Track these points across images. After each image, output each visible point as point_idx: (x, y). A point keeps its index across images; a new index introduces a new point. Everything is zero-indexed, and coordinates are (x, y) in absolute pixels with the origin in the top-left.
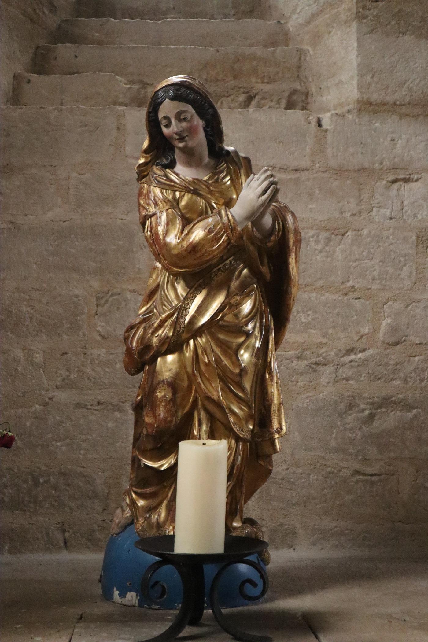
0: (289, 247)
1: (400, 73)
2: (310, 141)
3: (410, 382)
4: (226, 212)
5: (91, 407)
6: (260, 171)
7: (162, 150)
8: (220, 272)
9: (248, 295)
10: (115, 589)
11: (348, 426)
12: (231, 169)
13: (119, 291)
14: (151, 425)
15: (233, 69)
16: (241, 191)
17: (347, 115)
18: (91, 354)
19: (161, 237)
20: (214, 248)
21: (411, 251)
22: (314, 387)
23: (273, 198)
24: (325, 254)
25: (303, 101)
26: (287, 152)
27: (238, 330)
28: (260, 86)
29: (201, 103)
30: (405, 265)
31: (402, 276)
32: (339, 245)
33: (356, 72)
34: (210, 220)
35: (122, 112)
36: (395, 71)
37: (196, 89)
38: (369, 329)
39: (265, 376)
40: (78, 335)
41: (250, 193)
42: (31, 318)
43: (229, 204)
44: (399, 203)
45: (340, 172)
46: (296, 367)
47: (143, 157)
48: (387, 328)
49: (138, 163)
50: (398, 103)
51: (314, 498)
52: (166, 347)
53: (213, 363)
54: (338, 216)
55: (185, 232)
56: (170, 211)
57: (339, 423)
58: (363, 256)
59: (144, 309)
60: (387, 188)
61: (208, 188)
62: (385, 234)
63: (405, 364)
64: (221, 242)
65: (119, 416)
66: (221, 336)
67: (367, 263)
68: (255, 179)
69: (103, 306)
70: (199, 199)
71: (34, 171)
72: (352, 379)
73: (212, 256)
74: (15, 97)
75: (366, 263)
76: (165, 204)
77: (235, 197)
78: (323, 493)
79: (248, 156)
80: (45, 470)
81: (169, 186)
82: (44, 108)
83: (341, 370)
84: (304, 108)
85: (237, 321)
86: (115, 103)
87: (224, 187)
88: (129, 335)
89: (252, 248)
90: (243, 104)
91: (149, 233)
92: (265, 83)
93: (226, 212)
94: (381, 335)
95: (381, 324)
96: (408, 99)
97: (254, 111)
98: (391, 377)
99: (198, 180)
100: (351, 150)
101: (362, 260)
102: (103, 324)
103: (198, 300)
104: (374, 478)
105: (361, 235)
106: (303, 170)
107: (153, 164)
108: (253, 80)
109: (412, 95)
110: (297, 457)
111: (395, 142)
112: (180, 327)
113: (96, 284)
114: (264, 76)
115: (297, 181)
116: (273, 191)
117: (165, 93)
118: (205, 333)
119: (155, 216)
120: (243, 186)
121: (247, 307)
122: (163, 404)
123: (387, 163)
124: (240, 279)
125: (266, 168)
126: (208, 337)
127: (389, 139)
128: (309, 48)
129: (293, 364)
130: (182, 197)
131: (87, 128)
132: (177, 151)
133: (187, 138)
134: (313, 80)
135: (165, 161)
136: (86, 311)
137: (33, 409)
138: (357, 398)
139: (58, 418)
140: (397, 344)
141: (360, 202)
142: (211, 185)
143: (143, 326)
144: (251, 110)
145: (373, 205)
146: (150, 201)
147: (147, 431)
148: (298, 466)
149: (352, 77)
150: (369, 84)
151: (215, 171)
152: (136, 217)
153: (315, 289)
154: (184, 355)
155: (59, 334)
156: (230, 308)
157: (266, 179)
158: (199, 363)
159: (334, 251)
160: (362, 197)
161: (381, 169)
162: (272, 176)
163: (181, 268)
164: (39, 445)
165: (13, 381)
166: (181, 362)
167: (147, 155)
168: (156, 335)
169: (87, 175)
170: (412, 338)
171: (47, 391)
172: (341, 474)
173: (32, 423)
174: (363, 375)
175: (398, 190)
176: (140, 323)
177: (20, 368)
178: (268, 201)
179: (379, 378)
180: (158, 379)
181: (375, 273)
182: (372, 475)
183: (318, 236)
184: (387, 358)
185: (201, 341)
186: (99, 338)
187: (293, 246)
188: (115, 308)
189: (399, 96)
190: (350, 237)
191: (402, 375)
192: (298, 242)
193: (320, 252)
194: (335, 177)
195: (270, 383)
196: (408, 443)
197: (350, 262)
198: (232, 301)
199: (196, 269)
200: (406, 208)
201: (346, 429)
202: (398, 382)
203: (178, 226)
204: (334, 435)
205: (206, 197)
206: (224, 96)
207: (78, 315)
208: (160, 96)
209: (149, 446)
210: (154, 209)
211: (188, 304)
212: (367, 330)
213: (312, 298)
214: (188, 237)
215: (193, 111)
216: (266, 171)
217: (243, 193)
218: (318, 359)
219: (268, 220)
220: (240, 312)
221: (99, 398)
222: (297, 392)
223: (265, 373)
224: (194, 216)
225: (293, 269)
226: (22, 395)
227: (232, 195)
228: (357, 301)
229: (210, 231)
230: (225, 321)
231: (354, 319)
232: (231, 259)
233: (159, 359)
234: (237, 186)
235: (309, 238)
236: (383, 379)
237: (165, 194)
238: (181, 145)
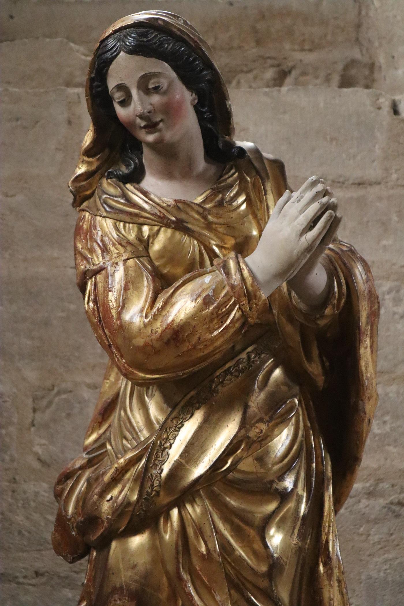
0: (359, 327)
2: (381, 137)
4: (238, 263)
6: (302, 183)
7: (118, 149)
8: (229, 377)
9: (283, 421)
12: (247, 181)
13: (69, 385)
15: (255, 30)
16: (266, 223)
18: (25, 492)
19: (114, 312)
20: (216, 333)
22: (395, 543)
23: (329, 234)
25: (366, 78)
26: (344, 156)
27: (265, 488)
28: (298, 56)
29: (188, 58)
34: (207, 279)
35: (76, 97)
37: (178, 33)
39: (318, 571)
41: (284, 226)
43: (243, 247)
46: (367, 510)
47: (83, 162)
49: (74, 172)
52: (126, 521)
53: (216, 555)
55: (159, 304)
56: (131, 262)
59: (94, 437)
61: (205, 218)
64: (228, 322)
65: (70, 595)
66: (233, 502)
68: (292, 200)
69: (43, 412)
70: (186, 239)
73: (211, 348)
76: (122, 250)
77: (255, 233)
79: (278, 157)
81: (133, 216)
84: (367, 87)
85: (262, 470)
86: (68, 84)
87: (234, 215)
88: (63, 490)
89: (289, 328)
90: (272, 83)
91: (91, 304)
97: (289, 90)
99: (184, 203)
102: (44, 441)
103: (189, 428)
106: (371, 184)
107: (103, 176)
108: (287, 46)
112: (152, 485)
113: (31, 374)
114: (304, 41)
115: (361, 202)
116: (328, 221)
117: (119, 40)
118: (201, 497)
119: (103, 272)
120: (271, 212)
121: (282, 441)
124: (269, 388)
125: (314, 178)
126: (207, 503)
129: (361, 505)
130: (154, 236)
131: (19, 123)
132: (146, 150)
133: (161, 125)
134: (381, 45)
135: (124, 170)
136: (15, 421)
142: (209, 211)
143: (88, 473)
144: (284, 89)
146: (95, 244)
151: (218, 187)
152: (72, 276)
153: (394, 379)
154: (161, 538)
156: (249, 447)
157: (314, 199)
158: (189, 555)
162: (326, 193)
163: (152, 372)
166: (155, 547)
167: (91, 159)
168: (109, 497)
169: (20, 198)
176: (83, 468)
178: (318, 242)
183: (398, 291)
185: (194, 511)
186: (36, 465)
187: (367, 324)
188: (64, 415)
192: (374, 315)
195: (326, 583)
198: (253, 433)
199: (180, 373)
203: (145, 291)
205: (200, 234)
206: (242, 71)
208: (109, 47)
210: (101, 259)
211: (167, 439)
213: (391, 395)
214: (164, 313)
215: (173, 75)
216: (314, 184)
217: (270, 227)
219: (318, 278)
220: (267, 453)
221: (38, 565)
223: (317, 565)
224: (178, 271)
225: (367, 367)
227: (250, 229)
229: (207, 302)
230: (239, 471)
232: (250, 349)
233: (114, 544)
234: (258, 213)
235: (384, 294)
237: (123, 232)
238: (151, 138)
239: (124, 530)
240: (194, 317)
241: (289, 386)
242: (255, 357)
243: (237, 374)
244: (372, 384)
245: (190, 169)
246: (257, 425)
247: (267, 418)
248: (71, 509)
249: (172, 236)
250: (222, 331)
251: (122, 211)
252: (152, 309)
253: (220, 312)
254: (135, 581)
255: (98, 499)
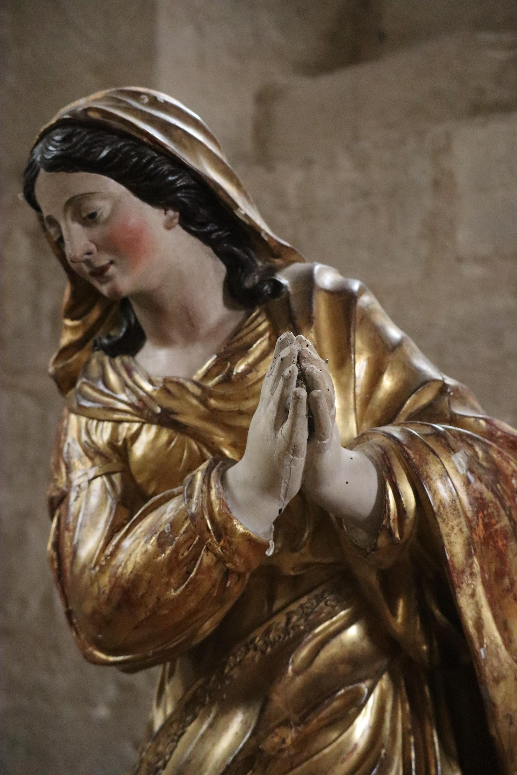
61: (204, 402)
133: (112, 270)
242: (298, 620)
244: (497, 655)
245: (193, 325)
246: (277, 730)
247: (297, 718)
249: (157, 436)
253: (180, 558)
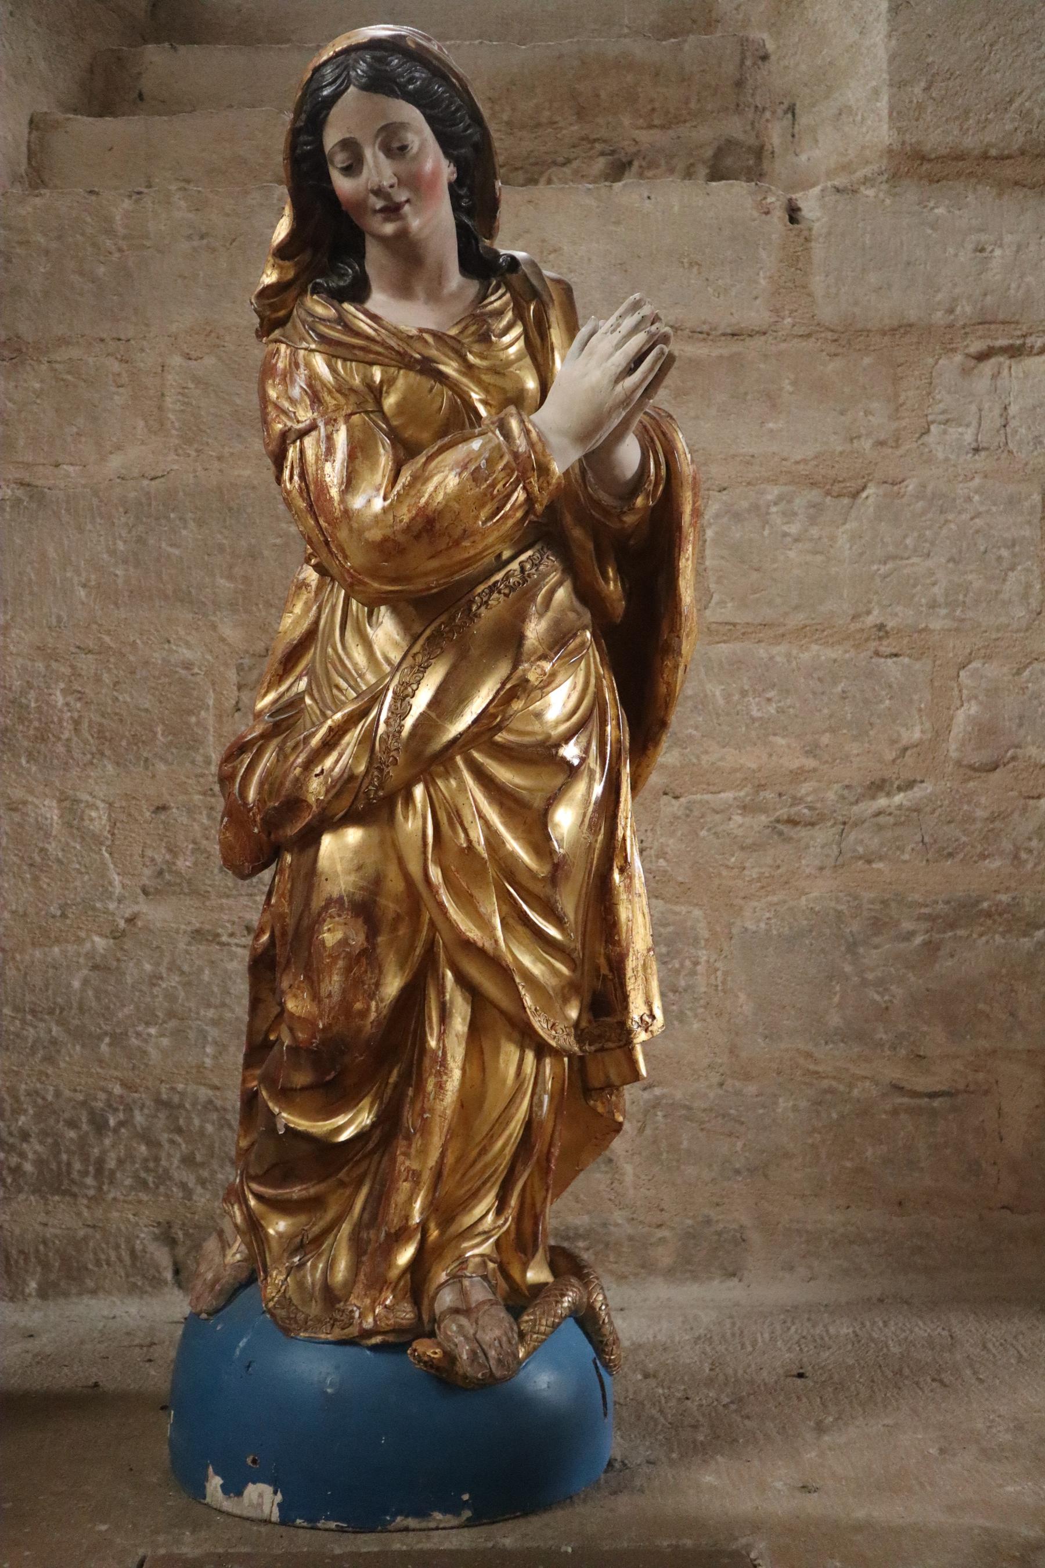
0: (679, 528)
1: (998, 75)
2: (769, 259)
3: (1026, 861)
5: (230, 940)
7: (330, 246)
8: (495, 595)
10: (211, 1469)
11: (870, 976)
14: (308, 1022)
17: (862, 188)
19: (334, 492)
21: (1027, 532)
22: (785, 879)
24: (808, 546)
29: (448, 106)
30: (1012, 569)
31: (1005, 596)
32: (844, 524)
33: (885, 76)
36: (985, 71)
38: (922, 732)
40: (193, 762)
41: (587, 368)
42: (77, 723)
44: (997, 411)
45: (848, 336)
46: (740, 832)
48: (969, 728)
50: (993, 152)
51: (787, 1155)
54: (839, 449)
55: (404, 478)
56: (356, 418)
57: (848, 969)
58: (906, 547)
60: (965, 372)
62: (961, 490)
63: (1016, 815)
67: (918, 565)
71: (75, 352)
72: (881, 858)
74: (37, 171)
75: (912, 565)
76: (342, 400)
78: (810, 1141)
80: (121, 1097)
82: (97, 194)
83: (852, 836)
92: (655, 126)
93: (522, 422)
94: (952, 748)
95: (952, 719)
96: (1020, 139)
98: (979, 848)
100: (873, 278)
101: (902, 558)
104: (936, 1103)
105: (899, 495)
109: (1030, 132)
110: (744, 1054)
111: (985, 255)
116: (654, 362)
119: (314, 433)
122: (341, 963)
123: (965, 309)
127: (970, 247)
128: (765, 36)
130: (389, 382)
133: (407, 208)
137: (88, 945)
138: (893, 905)
139: (148, 967)
140: (994, 767)
141: (897, 410)
145: (930, 418)
147: (294, 1037)
148: (747, 1077)
149: (876, 92)
150: (920, 107)
153: (783, 635)
155: (146, 760)
157: (635, 330)
159: (833, 538)
160: (901, 399)
161: (951, 326)
164: (106, 1034)
165: (36, 879)
167: (287, 263)
168: (318, 770)
169: (210, 361)
170: (1033, 751)
171: (120, 901)
172: (856, 1092)
173: (86, 982)
174: (909, 848)
175: (995, 377)
176: (266, 737)
177: (52, 847)
179: (950, 855)
180: (325, 895)
181: (936, 589)
182: (933, 1095)
183: (789, 502)
184: (969, 802)
189: (995, 134)
190: (870, 501)
191: (1007, 845)
193: (797, 540)
194: (833, 348)
195: (624, 896)
196: (1022, 1014)
197: (873, 562)
200: (1013, 424)
201: (864, 983)
202: (997, 863)
204: (836, 999)
206: (554, 163)
207: (190, 712)
209: (301, 1078)
212: (917, 735)
218: (794, 810)
219: (629, 454)
222: (742, 894)
224: (425, 436)
226: (59, 913)
228: (890, 661)
231: (882, 706)
232: (523, 557)
235: (768, 506)
236: (961, 856)
239: (341, 819)
240: (459, 496)
241: (578, 613)
243: (507, 591)
248: (252, 794)
250: (391, 592)
251: (339, 343)
252: (393, 487)
254: (362, 888)
255: (302, 773)
